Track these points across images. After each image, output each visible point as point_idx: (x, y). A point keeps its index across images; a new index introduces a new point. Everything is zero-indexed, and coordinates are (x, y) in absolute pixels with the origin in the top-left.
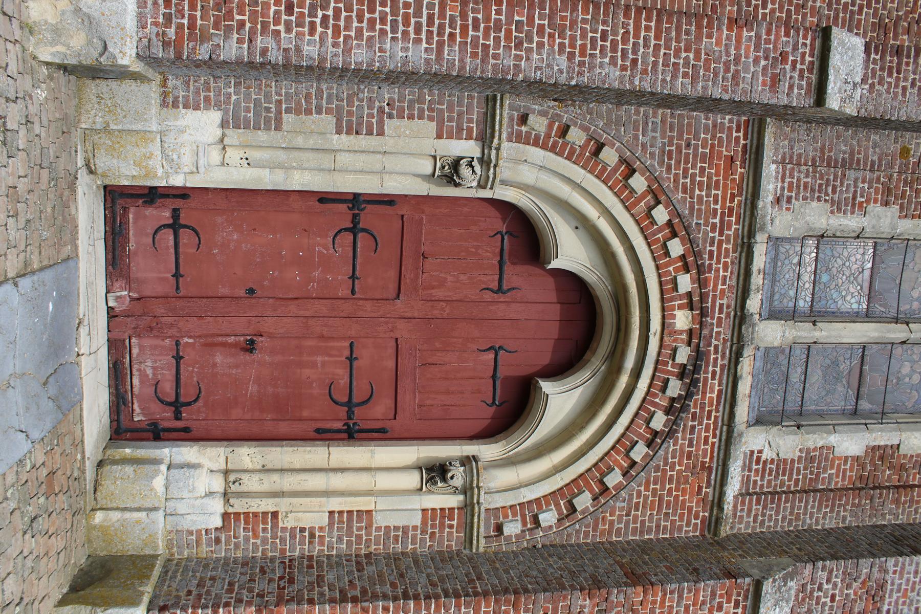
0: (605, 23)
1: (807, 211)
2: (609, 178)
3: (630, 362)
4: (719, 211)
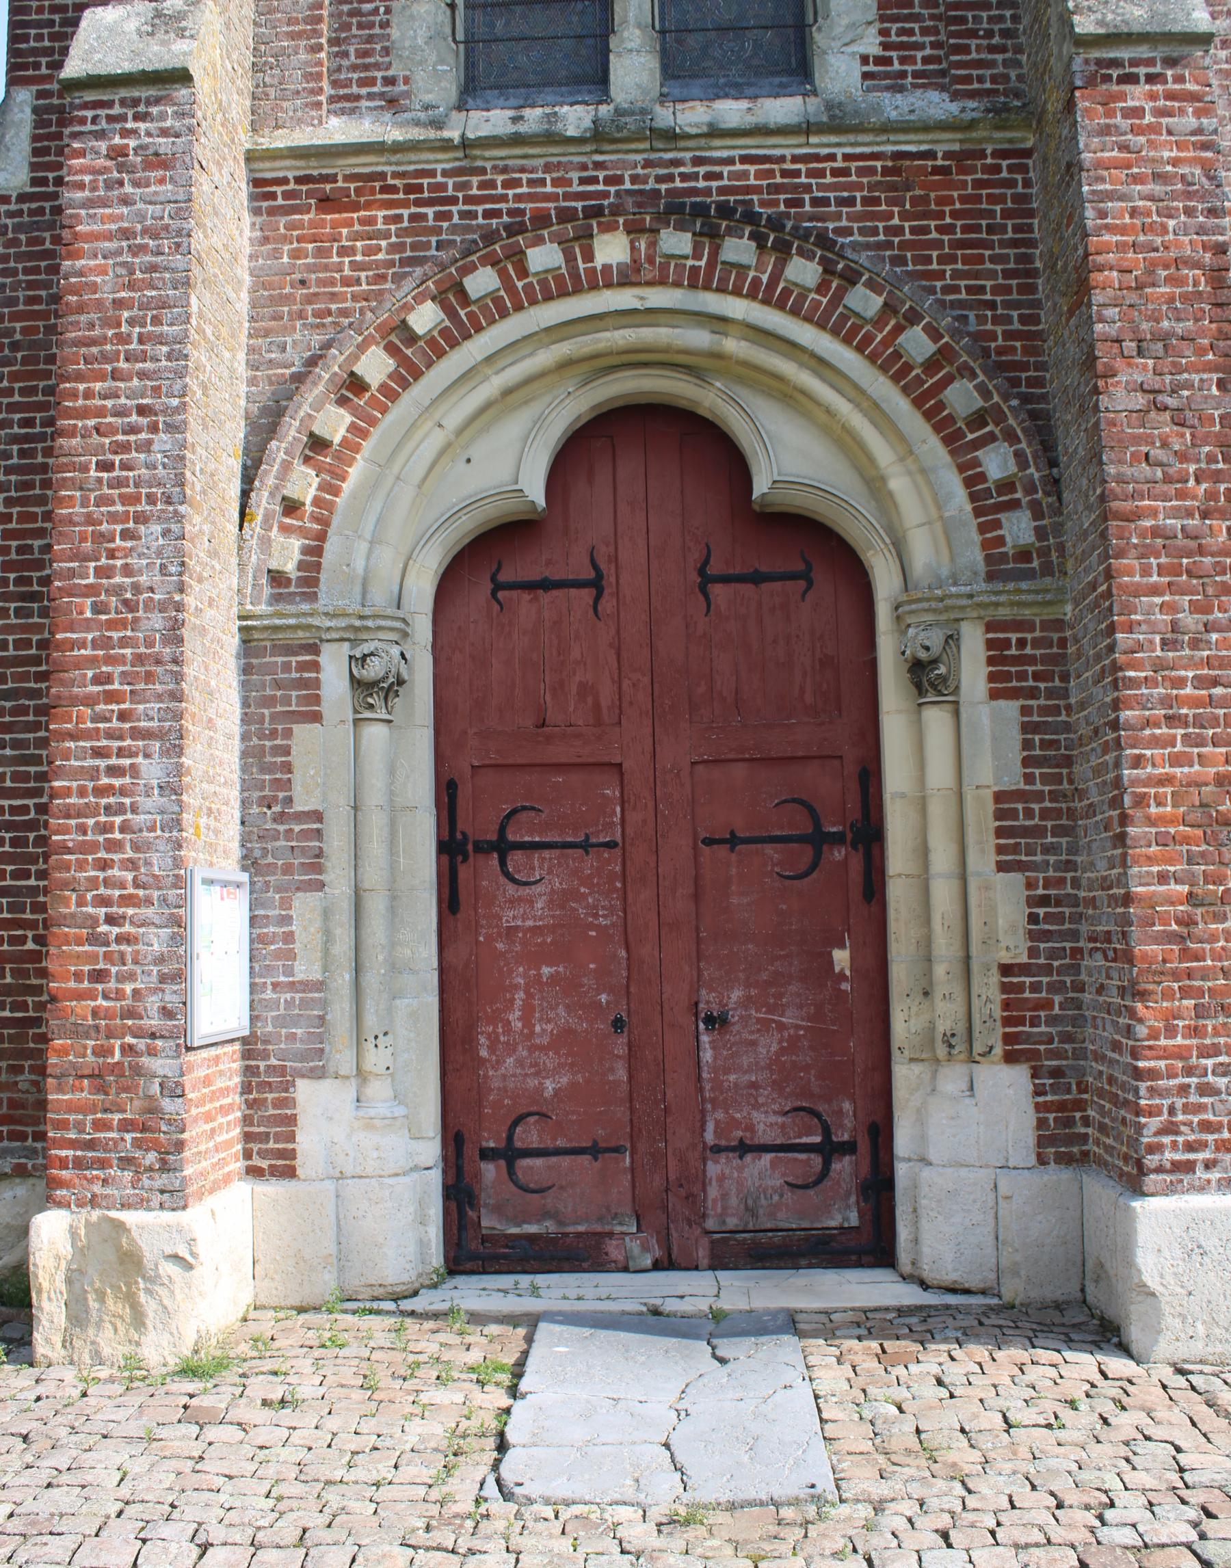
0: (85, 468)
1: (407, 44)
4: (414, 210)
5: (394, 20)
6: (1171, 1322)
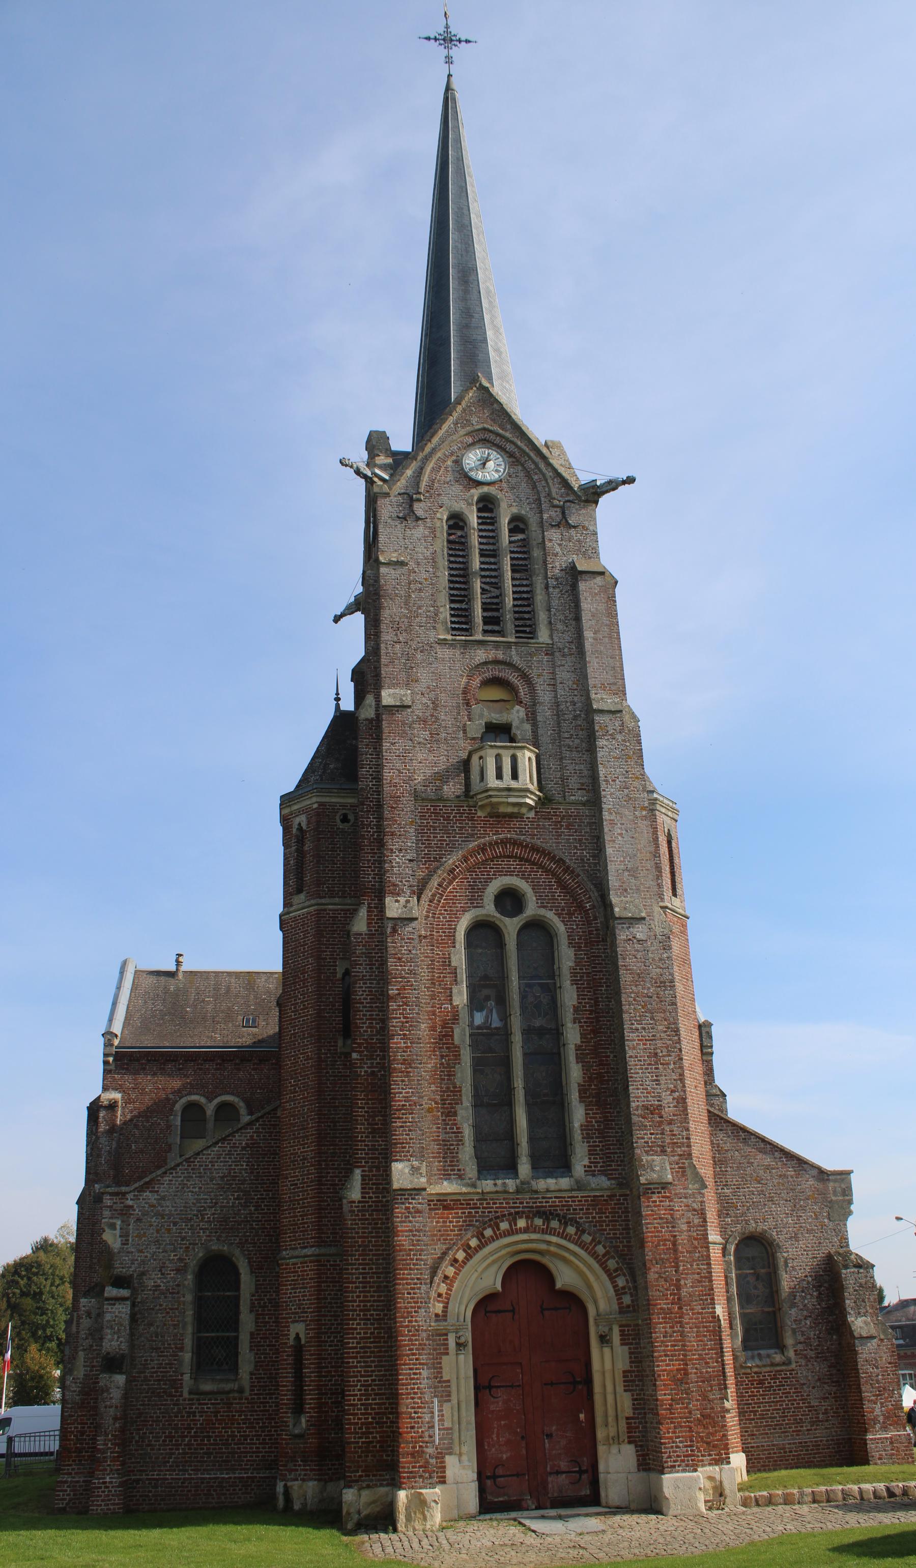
5: (460, 1152)
6: (672, 1505)
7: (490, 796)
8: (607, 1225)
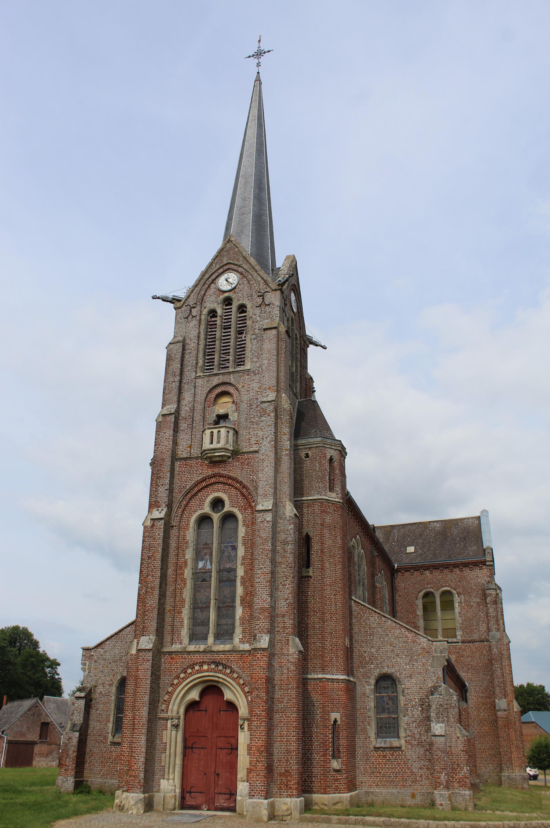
2: (175, 689)
3: (216, 679)
7: (206, 454)
8: (246, 669)
